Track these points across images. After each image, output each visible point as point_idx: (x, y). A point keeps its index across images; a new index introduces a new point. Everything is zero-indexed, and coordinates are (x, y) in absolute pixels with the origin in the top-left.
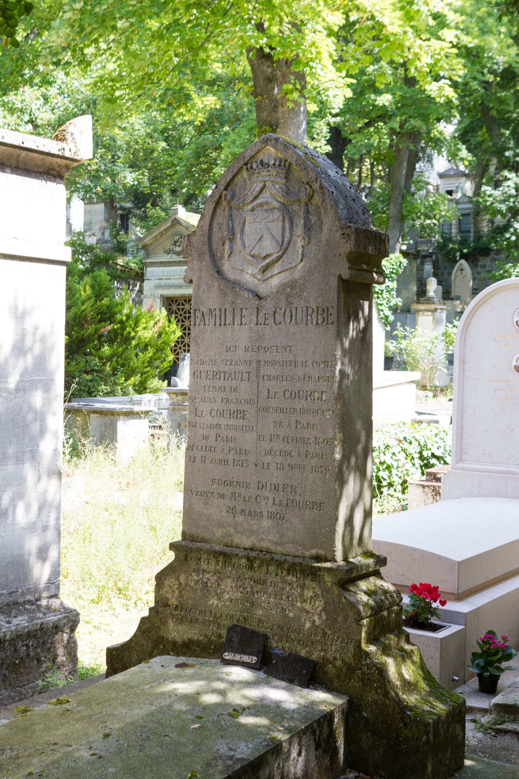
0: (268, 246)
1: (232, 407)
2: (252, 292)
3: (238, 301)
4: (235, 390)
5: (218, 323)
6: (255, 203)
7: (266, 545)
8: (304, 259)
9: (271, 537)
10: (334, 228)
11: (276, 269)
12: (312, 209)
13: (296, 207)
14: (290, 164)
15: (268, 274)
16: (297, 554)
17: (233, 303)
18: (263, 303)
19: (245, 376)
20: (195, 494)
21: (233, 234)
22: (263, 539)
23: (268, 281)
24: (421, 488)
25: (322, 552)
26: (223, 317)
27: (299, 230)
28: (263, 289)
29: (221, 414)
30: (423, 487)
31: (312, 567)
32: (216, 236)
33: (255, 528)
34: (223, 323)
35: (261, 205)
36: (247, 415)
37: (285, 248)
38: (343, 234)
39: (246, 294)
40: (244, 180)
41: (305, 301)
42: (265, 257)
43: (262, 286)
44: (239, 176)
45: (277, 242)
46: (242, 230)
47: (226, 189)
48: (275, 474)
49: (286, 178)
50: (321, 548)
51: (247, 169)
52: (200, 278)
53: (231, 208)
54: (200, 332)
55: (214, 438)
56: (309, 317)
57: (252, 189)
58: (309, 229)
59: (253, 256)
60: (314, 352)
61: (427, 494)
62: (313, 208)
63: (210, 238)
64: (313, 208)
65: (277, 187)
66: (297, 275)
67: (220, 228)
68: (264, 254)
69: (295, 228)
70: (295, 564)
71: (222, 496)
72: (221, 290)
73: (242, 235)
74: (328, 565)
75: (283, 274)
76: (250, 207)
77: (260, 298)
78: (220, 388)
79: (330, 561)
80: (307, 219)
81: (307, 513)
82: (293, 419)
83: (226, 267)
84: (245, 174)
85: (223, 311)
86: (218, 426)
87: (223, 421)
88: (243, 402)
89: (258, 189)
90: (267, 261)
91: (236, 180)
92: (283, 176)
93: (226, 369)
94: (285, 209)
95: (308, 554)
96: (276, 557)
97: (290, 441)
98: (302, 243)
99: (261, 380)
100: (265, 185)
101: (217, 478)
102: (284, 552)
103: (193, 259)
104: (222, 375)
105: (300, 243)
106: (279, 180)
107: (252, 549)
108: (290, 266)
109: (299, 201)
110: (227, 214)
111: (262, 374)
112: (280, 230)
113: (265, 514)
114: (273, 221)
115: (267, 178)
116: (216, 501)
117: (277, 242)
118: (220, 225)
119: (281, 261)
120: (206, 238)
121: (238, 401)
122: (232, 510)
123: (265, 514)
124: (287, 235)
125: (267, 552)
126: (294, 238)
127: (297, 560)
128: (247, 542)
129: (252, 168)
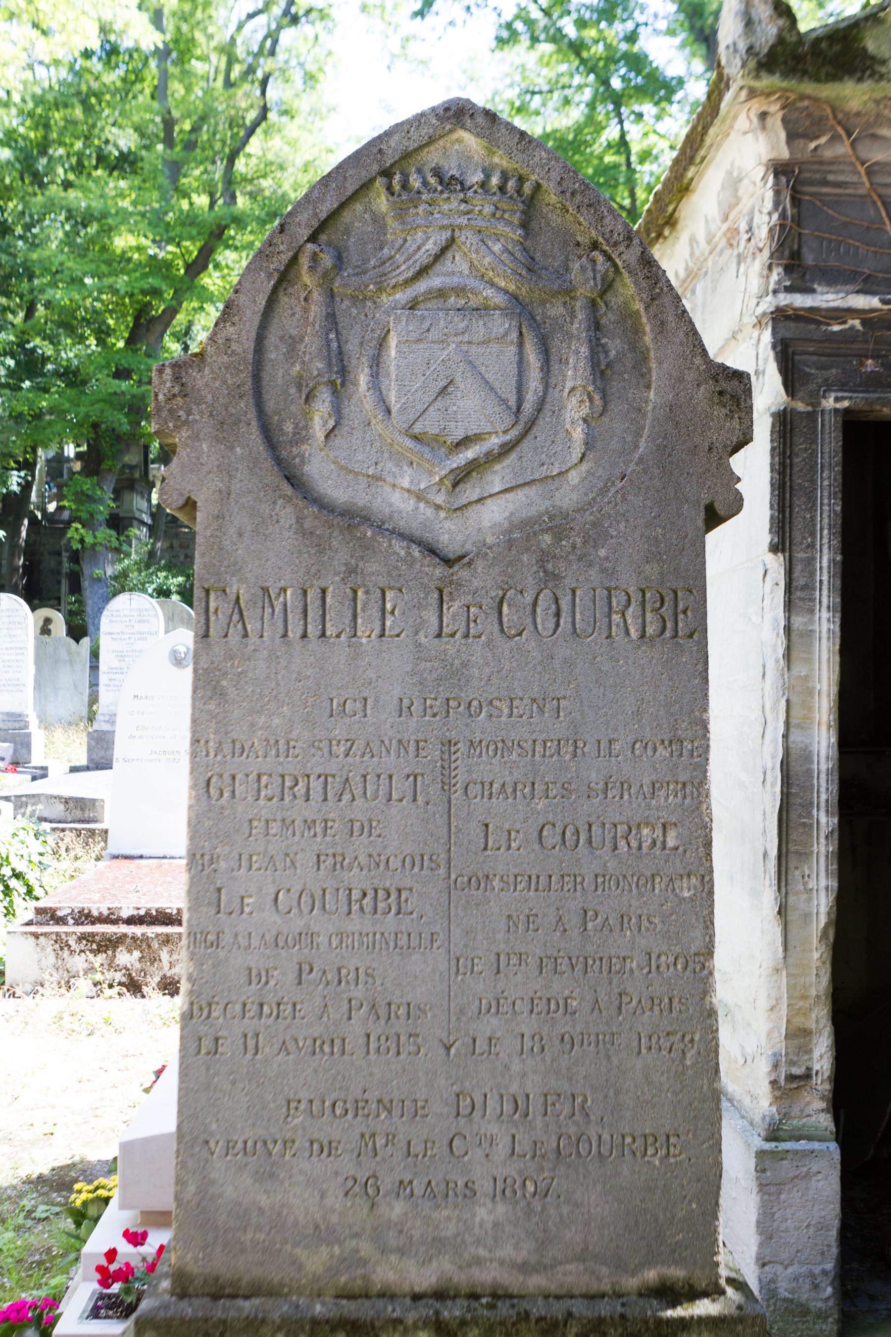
0: (474, 412)
1: (356, 879)
2: (411, 539)
3: (372, 567)
4: (367, 828)
5: (294, 632)
6: (422, 286)
7: (487, 1275)
8: (590, 456)
9: (507, 1251)
10: (690, 376)
11: (497, 478)
12: (608, 319)
13: (556, 310)
14: (538, 187)
15: (470, 492)
16: (595, 1287)
17: (352, 571)
18: (461, 573)
19: (400, 787)
20: (219, 1150)
21: (343, 371)
22: (478, 1261)
23: (470, 512)
24: (32, 939)
25: (677, 1273)
26: (313, 613)
27: (574, 372)
28: (450, 534)
29: (317, 901)
30: (36, 936)
31: (660, 1322)
32: (280, 373)
33: (450, 1230)
34: (313, 630)
35: (441, 294)
36: (412, 903)
37: (527, 421)
38: (721, 393)
39: (399, 547)
40: (378, 221)
41: (603, 571)
42: (465, 442)
43: (448, 525)
44: (358, 207)
45: (504, 401)
46: (376, 363)
47: (313, 238)
48: (516, 1068)
49: (524, 225)
50: (675, 1263)
51: (389, 189)
52: (225, 495)
53: (331, 295)
54: (230, 656)
55: (292, 976)
56: (616, 618)
57: (411, 246)
58: (602, 373)
59: (416, 438)
60: (638, 713)
61: (43, 949)
62: (612, 317)
63: (257, 378)
64: (612, 317)
65: (497, 247)
66: (568, 496)
67: (292, 352)
68: (459, 434)
69: (555, 367)
70: (601, 1321)
71: (327, 1148)
72: (304, 533)
73: (375, 376)
74: (704, 1308)
75: (520, 494)
76: (401, 297)
77: (448, 562)
78: (309, 824)
79: (705, 1294)
80: (596, 348)
81: (625, 1171)
82: (574, 905)
83: (320, 468)
84: (382, 202)
85: (313, 595)
86: (308, 937)
87: (324, 926)
88: (395, 863)
89: (431, 247)
90: (470, 454)
91: (347, 216)
92: (516, 219)
93: (332, 767)
94: (521, 309)
95: (631, 1283)
96: (538, 1309)
97: (564, 965)
98: (585, 410)
99: (457, 795)
100: (451, 241)
101: (304, 1095)
102: (553, 1288)
103: (196, 437)
104: (316, 785)
105: (574, 410)
106: (501, 228)
107: (440, 1295)
108: (544, 471)
109: (569, 292)
110: (316, 310)
111: (461, 779)
112: (513, 369)
113: (484, 1186)
114: (486, 342)
115: (463, 220)
116: (306, 1165)
117: (504, 401)
118: (293, 344)
119: (513, 456)
120: (245, 376)
121: (377, 862)
122: (367, 1189)
123: (484, 1186)
124: (534, 384)
125: (495, 1296)
126: (553, 394)
127: (604, 1309)
128: (424, 1278)
129: (405, 186)
